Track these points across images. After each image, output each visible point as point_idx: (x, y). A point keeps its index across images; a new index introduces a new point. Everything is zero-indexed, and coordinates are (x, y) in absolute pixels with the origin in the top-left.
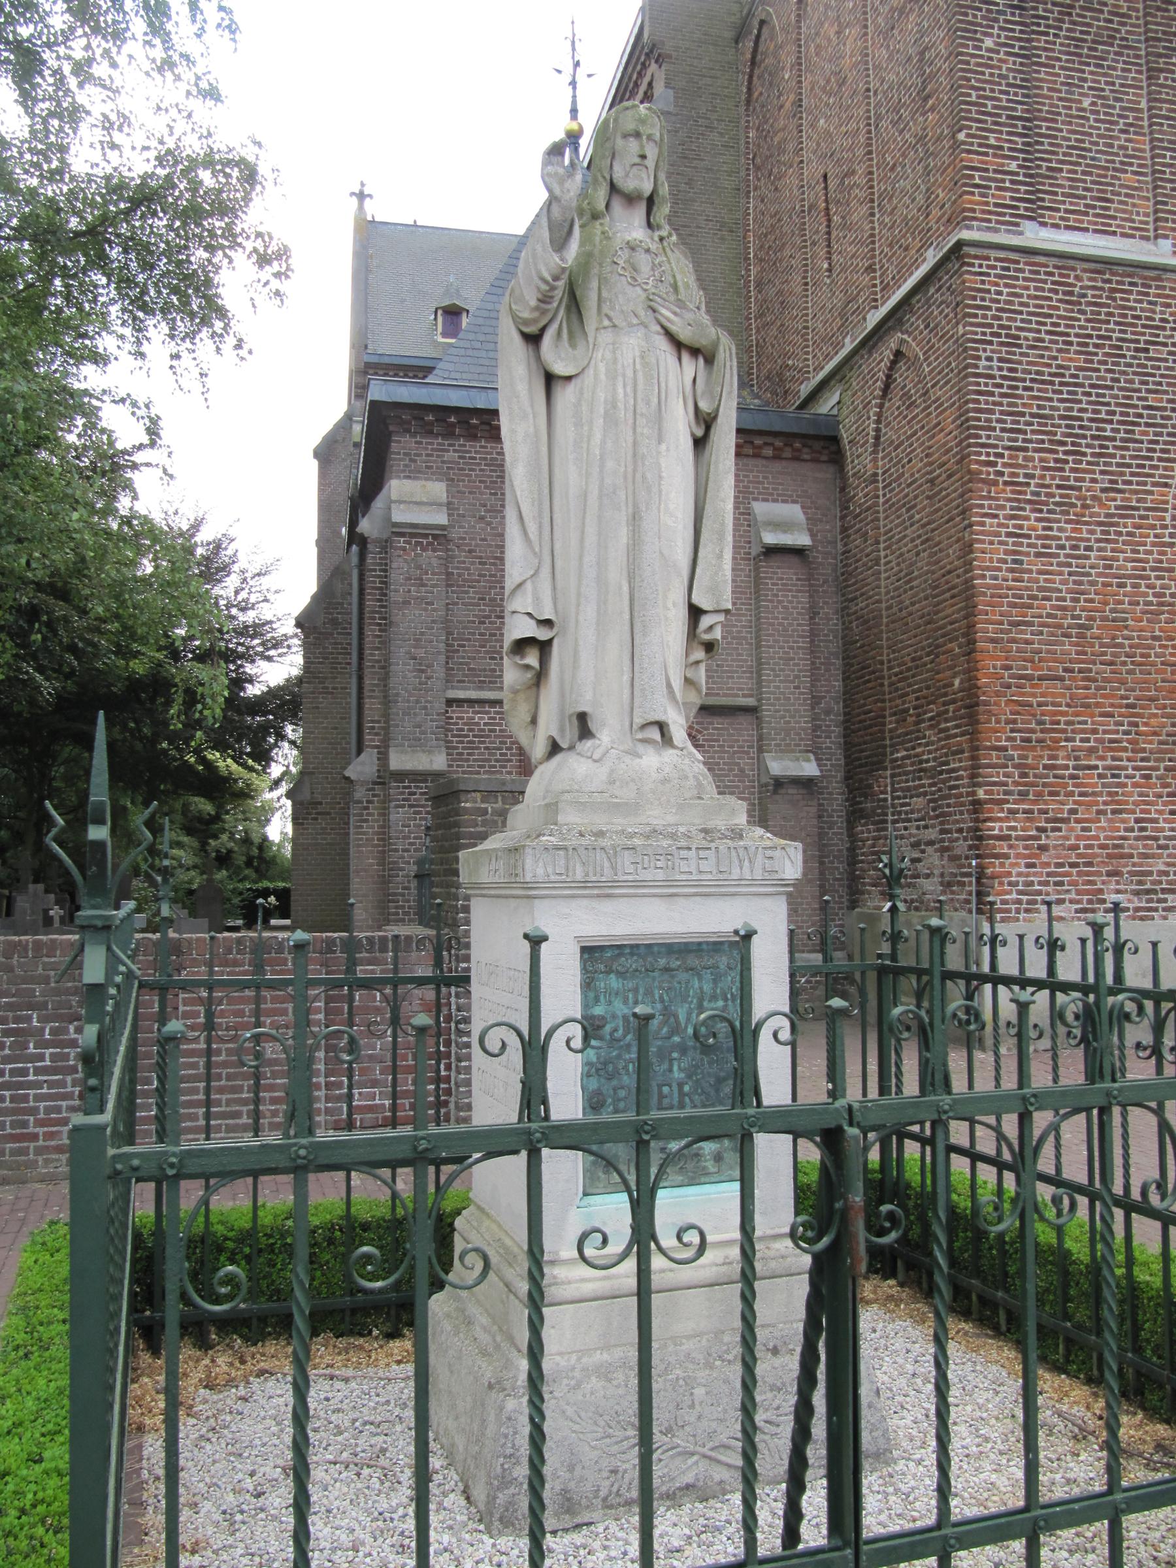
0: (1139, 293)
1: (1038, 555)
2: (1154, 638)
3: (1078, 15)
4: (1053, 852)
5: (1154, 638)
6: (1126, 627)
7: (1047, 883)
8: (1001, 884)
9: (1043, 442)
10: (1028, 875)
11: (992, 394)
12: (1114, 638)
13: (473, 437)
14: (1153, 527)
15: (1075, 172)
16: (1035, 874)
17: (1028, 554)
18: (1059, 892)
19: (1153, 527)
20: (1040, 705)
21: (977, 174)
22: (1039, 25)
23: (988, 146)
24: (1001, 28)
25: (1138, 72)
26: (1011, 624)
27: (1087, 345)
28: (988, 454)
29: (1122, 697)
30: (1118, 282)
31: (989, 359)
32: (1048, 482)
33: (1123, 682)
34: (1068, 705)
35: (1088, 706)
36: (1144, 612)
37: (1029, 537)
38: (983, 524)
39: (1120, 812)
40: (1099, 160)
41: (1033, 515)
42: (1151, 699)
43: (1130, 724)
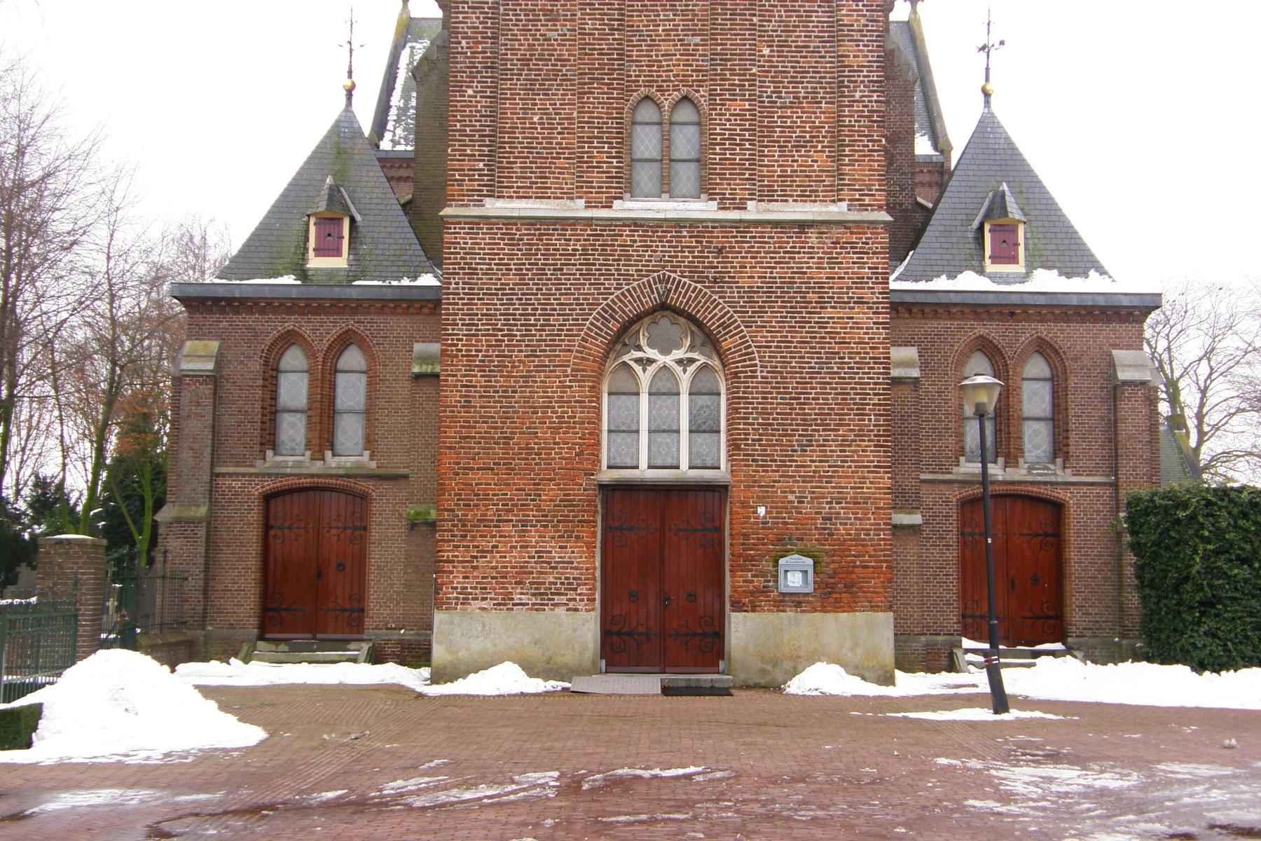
0: (558, 235)
1: (481, 397)
2: (555, 443)
3: (534, 65)
4: (481, 570)
5: (555, 443)
6: (537, 437)
7: (476, 588)
8: (447, 588)
9: (489, 330)
10: (464, 583)
11: (457, 304)
12: (527, 444)
13: (238, 313)
14: (558, 377)
15: (526, 163)
16: (468, 583)
17: (475, 397)
18: (483, 594)
19: (558, 377)
20: (477, 484)
21: (457, 173)
22: (506, 75)
23: (465, 155)
24: (478, 82)
25: (572, 95)
26: (460, 438)
27: (522, 269)
28: (453, 340)
29: (531, 479)
30: (545, 230)
31: (456, 283)
32: (490, 353)
33: (533, 470)
34: (495, 484)
35: (509, 484)
36: (549, 428)
37: (476, 387)
38: (447, 381)
39: (527, 547)
40: (542, 153)
41: (479, 374)
42: (551, 480)
43: (535, 495)
